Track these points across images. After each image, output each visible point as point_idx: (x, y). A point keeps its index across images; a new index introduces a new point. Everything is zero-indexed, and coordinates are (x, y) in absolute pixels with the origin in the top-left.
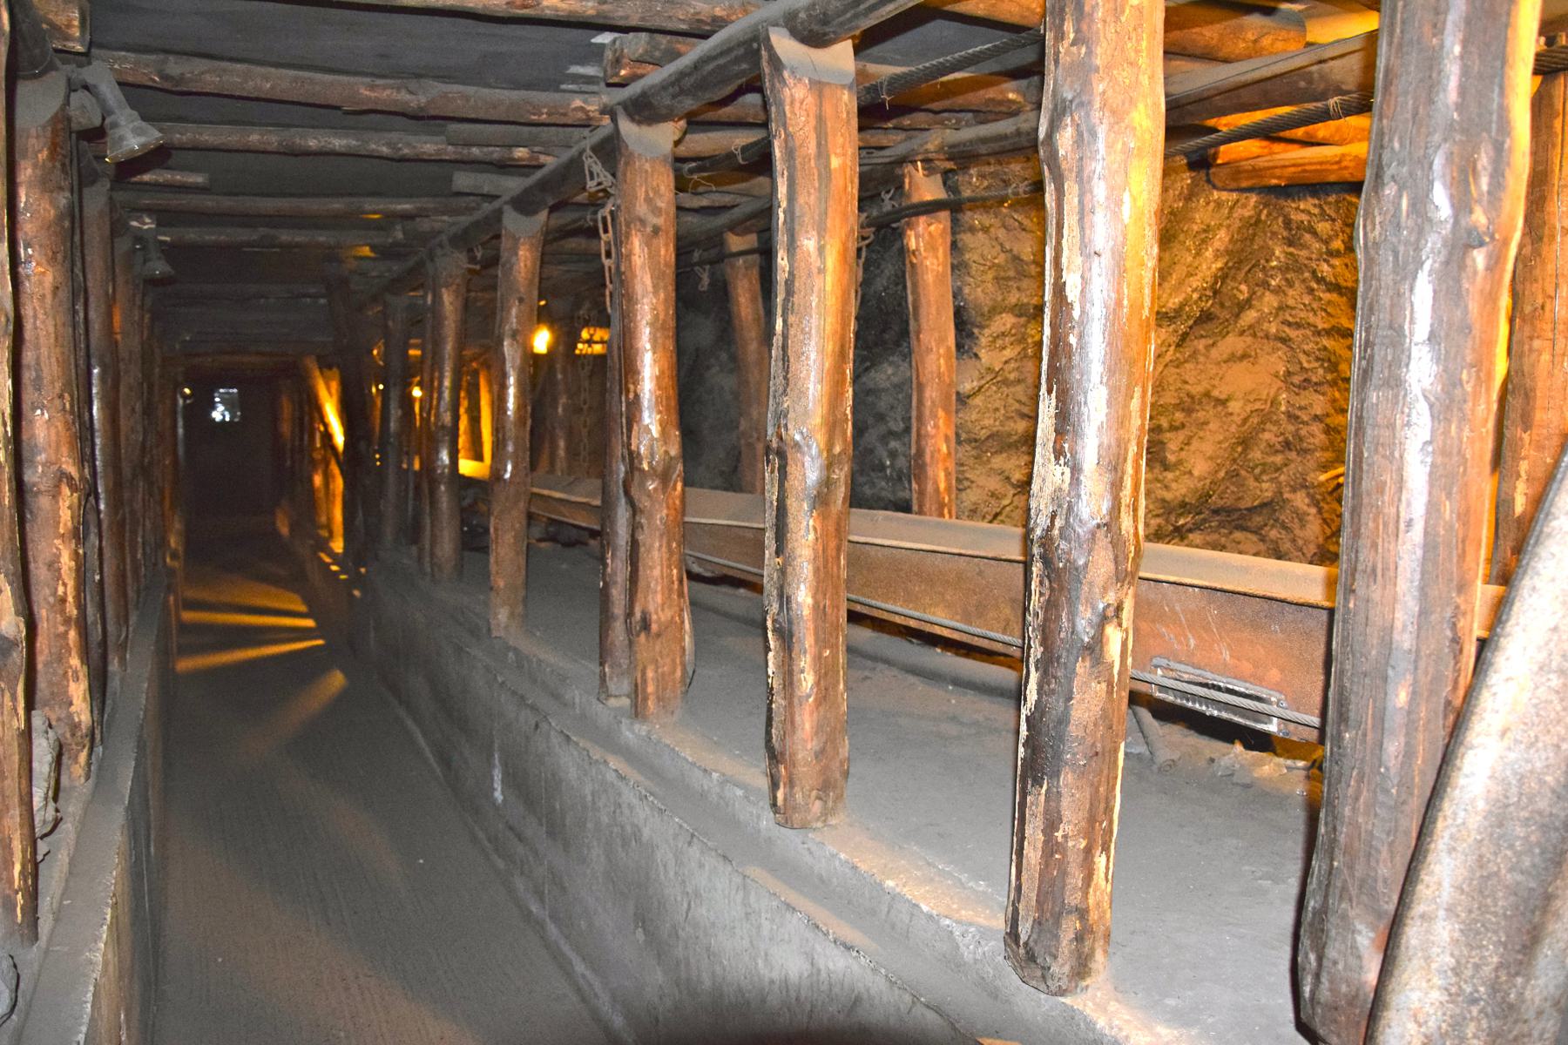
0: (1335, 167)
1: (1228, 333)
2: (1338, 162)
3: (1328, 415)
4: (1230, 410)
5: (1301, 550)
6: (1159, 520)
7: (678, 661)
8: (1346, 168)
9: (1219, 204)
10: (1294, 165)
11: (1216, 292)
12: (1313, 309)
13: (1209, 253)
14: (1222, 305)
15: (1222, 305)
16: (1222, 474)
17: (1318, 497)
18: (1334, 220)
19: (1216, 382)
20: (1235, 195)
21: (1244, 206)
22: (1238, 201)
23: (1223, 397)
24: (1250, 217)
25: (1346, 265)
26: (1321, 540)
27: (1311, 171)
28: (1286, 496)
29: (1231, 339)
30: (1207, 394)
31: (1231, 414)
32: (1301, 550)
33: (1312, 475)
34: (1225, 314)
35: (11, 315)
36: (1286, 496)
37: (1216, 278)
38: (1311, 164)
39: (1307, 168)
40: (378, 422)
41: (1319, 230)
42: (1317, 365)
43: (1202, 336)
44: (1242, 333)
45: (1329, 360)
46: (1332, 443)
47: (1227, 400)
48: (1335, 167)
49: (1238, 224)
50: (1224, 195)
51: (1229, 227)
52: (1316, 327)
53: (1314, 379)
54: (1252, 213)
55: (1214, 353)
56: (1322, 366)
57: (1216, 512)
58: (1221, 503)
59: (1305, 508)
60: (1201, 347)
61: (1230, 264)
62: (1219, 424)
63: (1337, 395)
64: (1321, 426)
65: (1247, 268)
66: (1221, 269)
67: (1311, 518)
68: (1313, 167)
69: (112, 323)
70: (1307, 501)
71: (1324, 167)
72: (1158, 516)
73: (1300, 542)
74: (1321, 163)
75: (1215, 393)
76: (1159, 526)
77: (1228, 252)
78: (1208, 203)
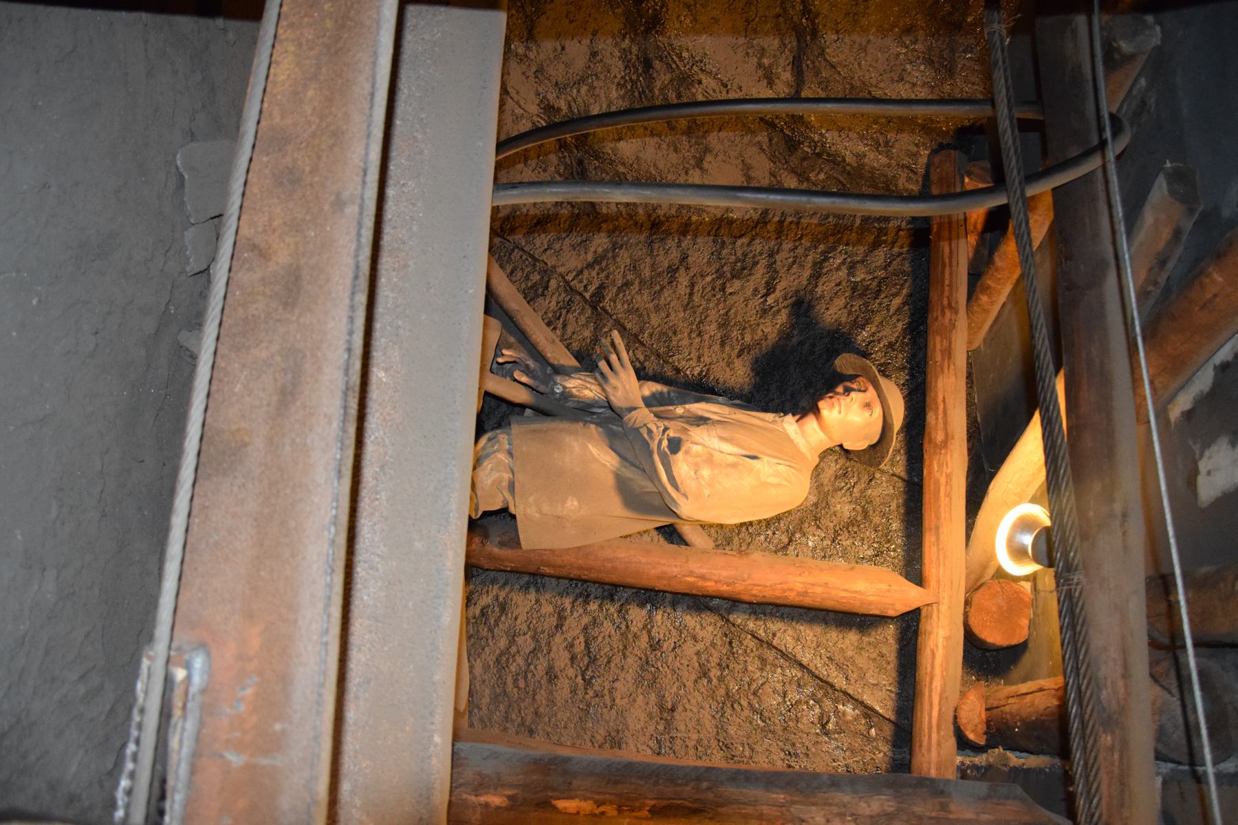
0: (945, 302)
1: (775, 163)
2: (950, 304)
3: (687, 268)
4: (691, 172)
5: (549, 248)
6: (564, 108)
7: (607, 797)
8: (943, 314)
9: (914, 155)
10: (951, 253)
11: (819, 155)
12: (796, 248)
13: (862, 148)
14: (804, 159)
15: (804, 159)
16: (621, 169)
17: (604, 264)
18: (885, 268)
19: (721, 157)
20: (921, 171)
21: (909, 179)
22: (916, 173)
23: (706, 165)
24: (896, 186)
25: (839, 284)
26: (561, 270)
27: (943, 273)
28: (604, 226)
29: (768, 165)
30: (707, 150)
31: (687, 173)
32: (549, 248)
33: (626, 255)
34: (794, 161)
35: (1180, 720)
36: (604, 226)
37: (837, 154)
38: (951, 274)
39: (947, 270)
40: (926, 724)
41: (876, 252)
42: (739, 253)
43: (770, 140)
44: (772, 174)
45: (743, 269)
46: (659, 275)
47: (701, 168)
48: (945, 302)
49: (890, 174)
50: (923, 160)
51: (889, 166)
52: (778, 252)
53: (724, 252)
54: (901, 186)
55: (754, 150)
56: (738, 260)
57: (580, 162)
58: (591, 168)
59: (592, 249)
60: (759, 138)
61: (848, 168)
62: (675, 162)
63: (709, 279)
64: (677, 262)
65: (841, 179)
66: (844, 160)
67: (583, 255)
68: (947, 276)
69: (1079, 155)
70: (600, 250)
71: (947, 288)
72: (570, 107)
73: (557, 246)
74: (950, 285)
75: (709, 158)
76: (559, 110)
77: (861, 166)
78: (917, 145)
